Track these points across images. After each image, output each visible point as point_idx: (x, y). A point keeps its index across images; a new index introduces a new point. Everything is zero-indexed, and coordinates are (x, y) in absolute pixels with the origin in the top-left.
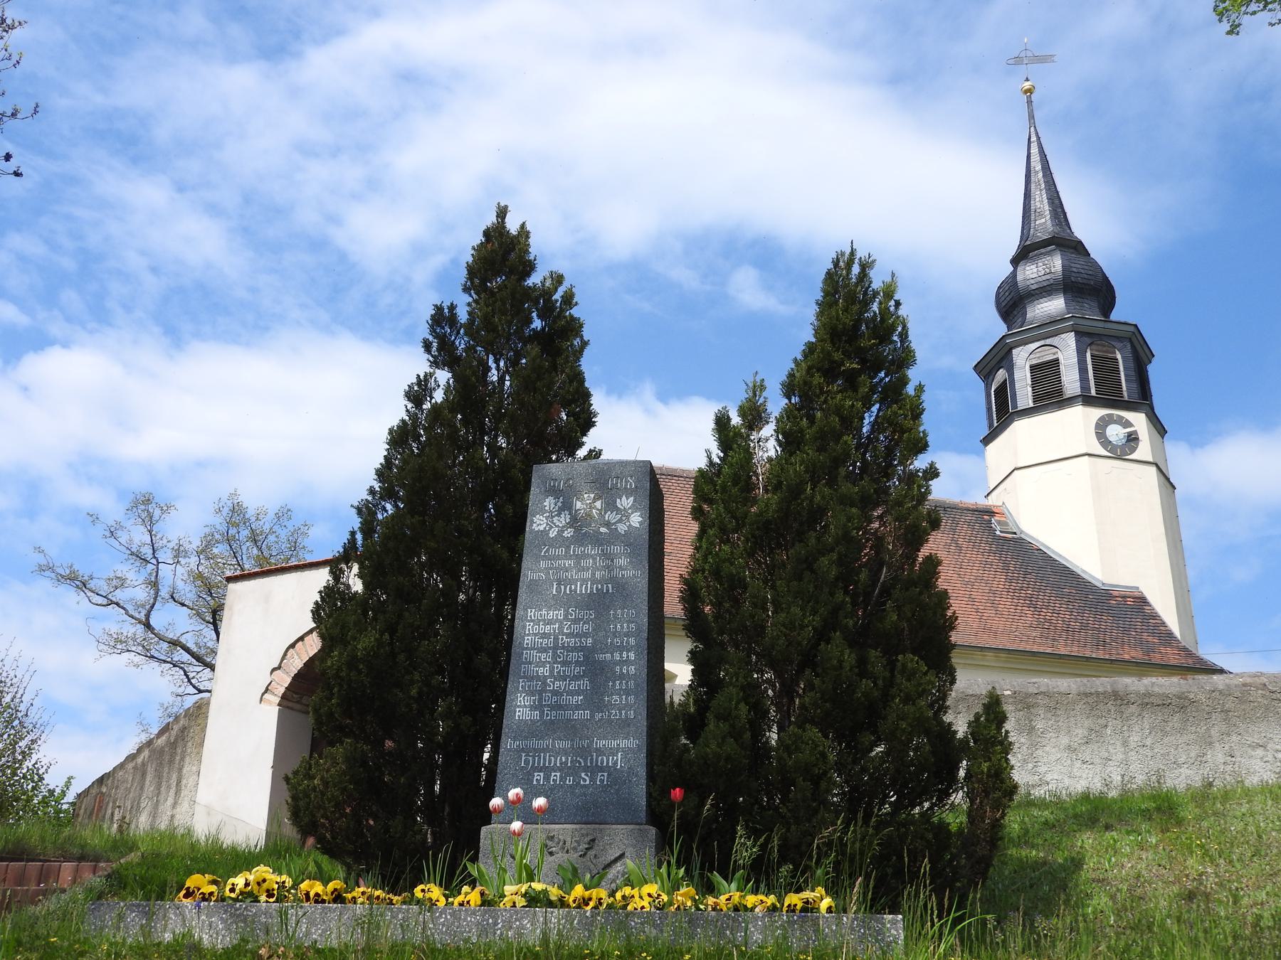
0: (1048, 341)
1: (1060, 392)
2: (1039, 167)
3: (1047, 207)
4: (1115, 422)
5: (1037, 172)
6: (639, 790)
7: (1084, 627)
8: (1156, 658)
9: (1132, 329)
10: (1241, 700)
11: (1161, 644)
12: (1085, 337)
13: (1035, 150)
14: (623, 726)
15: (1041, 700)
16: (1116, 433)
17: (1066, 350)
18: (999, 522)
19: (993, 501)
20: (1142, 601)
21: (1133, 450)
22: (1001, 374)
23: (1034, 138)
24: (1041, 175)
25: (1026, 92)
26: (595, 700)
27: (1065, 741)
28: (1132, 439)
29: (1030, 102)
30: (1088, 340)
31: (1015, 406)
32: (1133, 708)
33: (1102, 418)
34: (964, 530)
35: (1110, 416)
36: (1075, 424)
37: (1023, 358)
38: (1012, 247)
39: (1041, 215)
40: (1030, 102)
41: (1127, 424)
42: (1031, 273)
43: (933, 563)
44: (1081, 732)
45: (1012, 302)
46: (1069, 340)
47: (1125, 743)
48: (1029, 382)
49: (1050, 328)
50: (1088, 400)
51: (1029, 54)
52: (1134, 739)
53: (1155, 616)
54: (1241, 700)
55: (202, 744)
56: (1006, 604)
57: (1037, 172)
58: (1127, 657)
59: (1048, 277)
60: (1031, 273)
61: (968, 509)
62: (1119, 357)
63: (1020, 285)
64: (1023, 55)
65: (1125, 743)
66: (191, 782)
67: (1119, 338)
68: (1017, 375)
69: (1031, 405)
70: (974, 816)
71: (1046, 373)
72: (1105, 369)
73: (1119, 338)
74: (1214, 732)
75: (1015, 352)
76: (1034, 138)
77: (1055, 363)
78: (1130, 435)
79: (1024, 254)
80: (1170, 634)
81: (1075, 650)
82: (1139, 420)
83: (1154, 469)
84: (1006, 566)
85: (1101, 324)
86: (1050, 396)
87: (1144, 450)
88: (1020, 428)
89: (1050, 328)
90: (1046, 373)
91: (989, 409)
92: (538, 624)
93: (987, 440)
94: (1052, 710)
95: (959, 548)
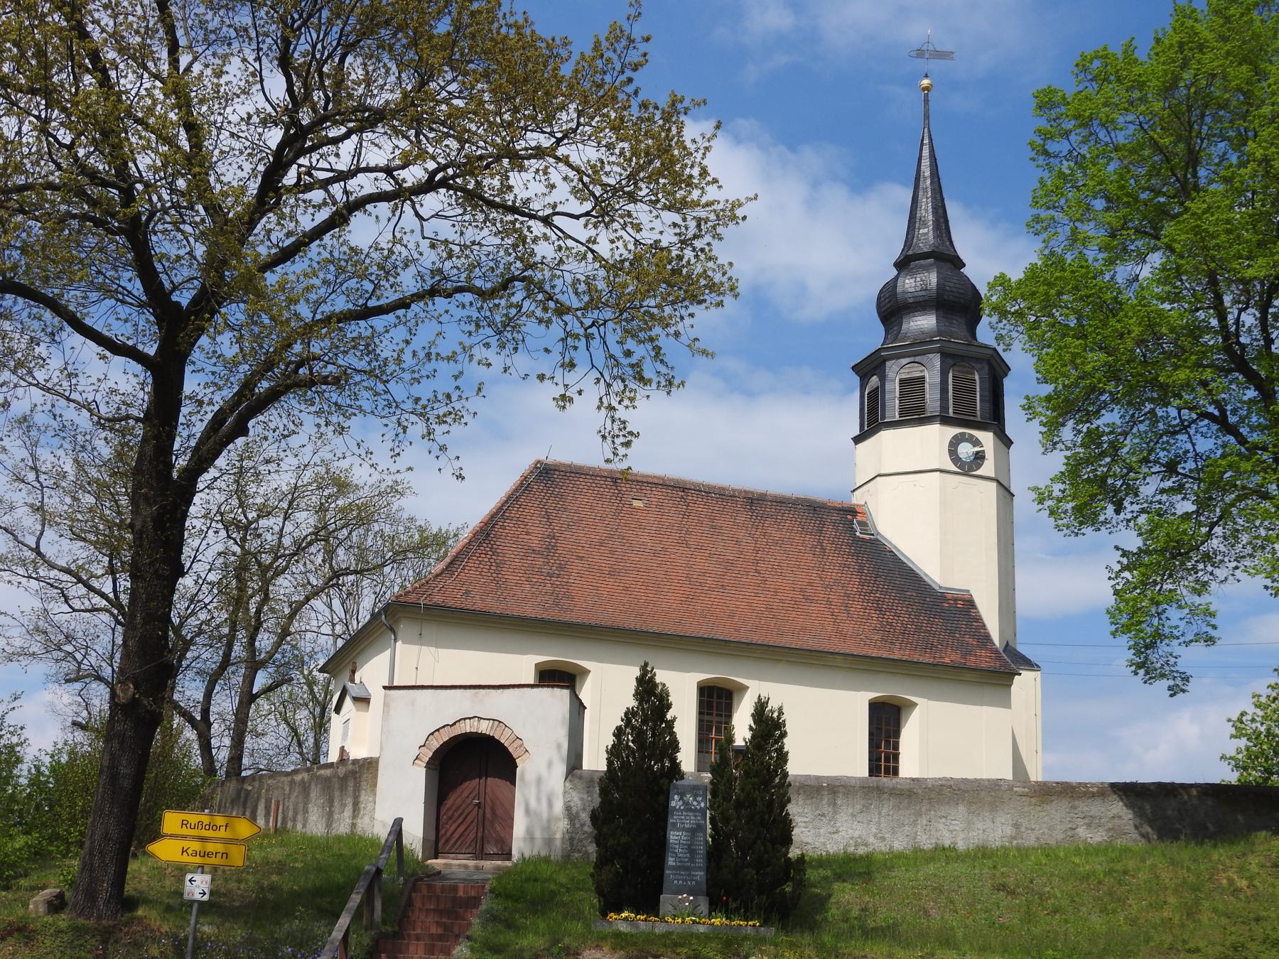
0: (917, 359)
1: (922, 409)
2: (927, 174)
3: (930, 217)
4: (967, 441)
5: (925, 178)
6: (704, 886)
7: (918, 629)
8: (971, 661)
9: (991, 352)
10: (939, 794)
11: (978, 646)
12: (950, 359)
13: (926, 152)
14: (700, 869)
15: (841, 789)
16: (966, 450)
17: (931, 372)
18: (861, 523)
19: (857, 499)
20: (970, 603)
21: (979, 466)
22: (874, 380)
23: (926, 141)
24: (928, 182)
25: (924, 89)
26: (692, 859)
27: (850, 811)
28: (979, 457)
29: (926, 100)
30: (951, 361)
31: (884, 417)
32: (886, 796)
33: (955, 437)
34: (829, 531)
35: (963, 434)
36: (930, 441)
37: (896, 372)
38: (897, 251)
39: (925, 225)
40: (926, 100)
41: (976, 442)
42: (909, 284)
43: (788, 814)
44: (859, 807)
45: (892, 308)
46: (936, 361)
47: (880, 813)
48: (897, 394)
49: (919, 347)
50: (945, 420)
51: (931, 48)
52: (884, 811)
53: (978, 619)
54: (939, 794)
55: (375, 785)
56: (857, 606)
57: (925, 178)
58: (947, 660)
59: (923, 293)
60: (909, 284)
61: (835, 509)
62: (977, 377)
63: (899, 289)
64: (925, 48)
65: (880, 813)
66: (369, 806)
67: (977, 360)
68: (888, 387)
69: (897, 418)
70: (794, 891)
71: (912, 386)
72: (964, 390)
73: (977, 360)
74: (923, 809)
75: (888, 364)
76: (926, 141)
77: (924, 377)
78: (977, 453)
79: (904, 264)
80: (988, 637)
81: (905, 655)
82: (987, 438)
83: (994, 484)
84: (861, 571)
85: (964, 348)
86: (914, 415)
87: (988, 468)
88: (886, 436)
89: (919, 347)
90: (912, 386)
91: (862, 409)
92: (674, 837)
93: (858, 440)
94: (846, 794)
95: (824, 549)
